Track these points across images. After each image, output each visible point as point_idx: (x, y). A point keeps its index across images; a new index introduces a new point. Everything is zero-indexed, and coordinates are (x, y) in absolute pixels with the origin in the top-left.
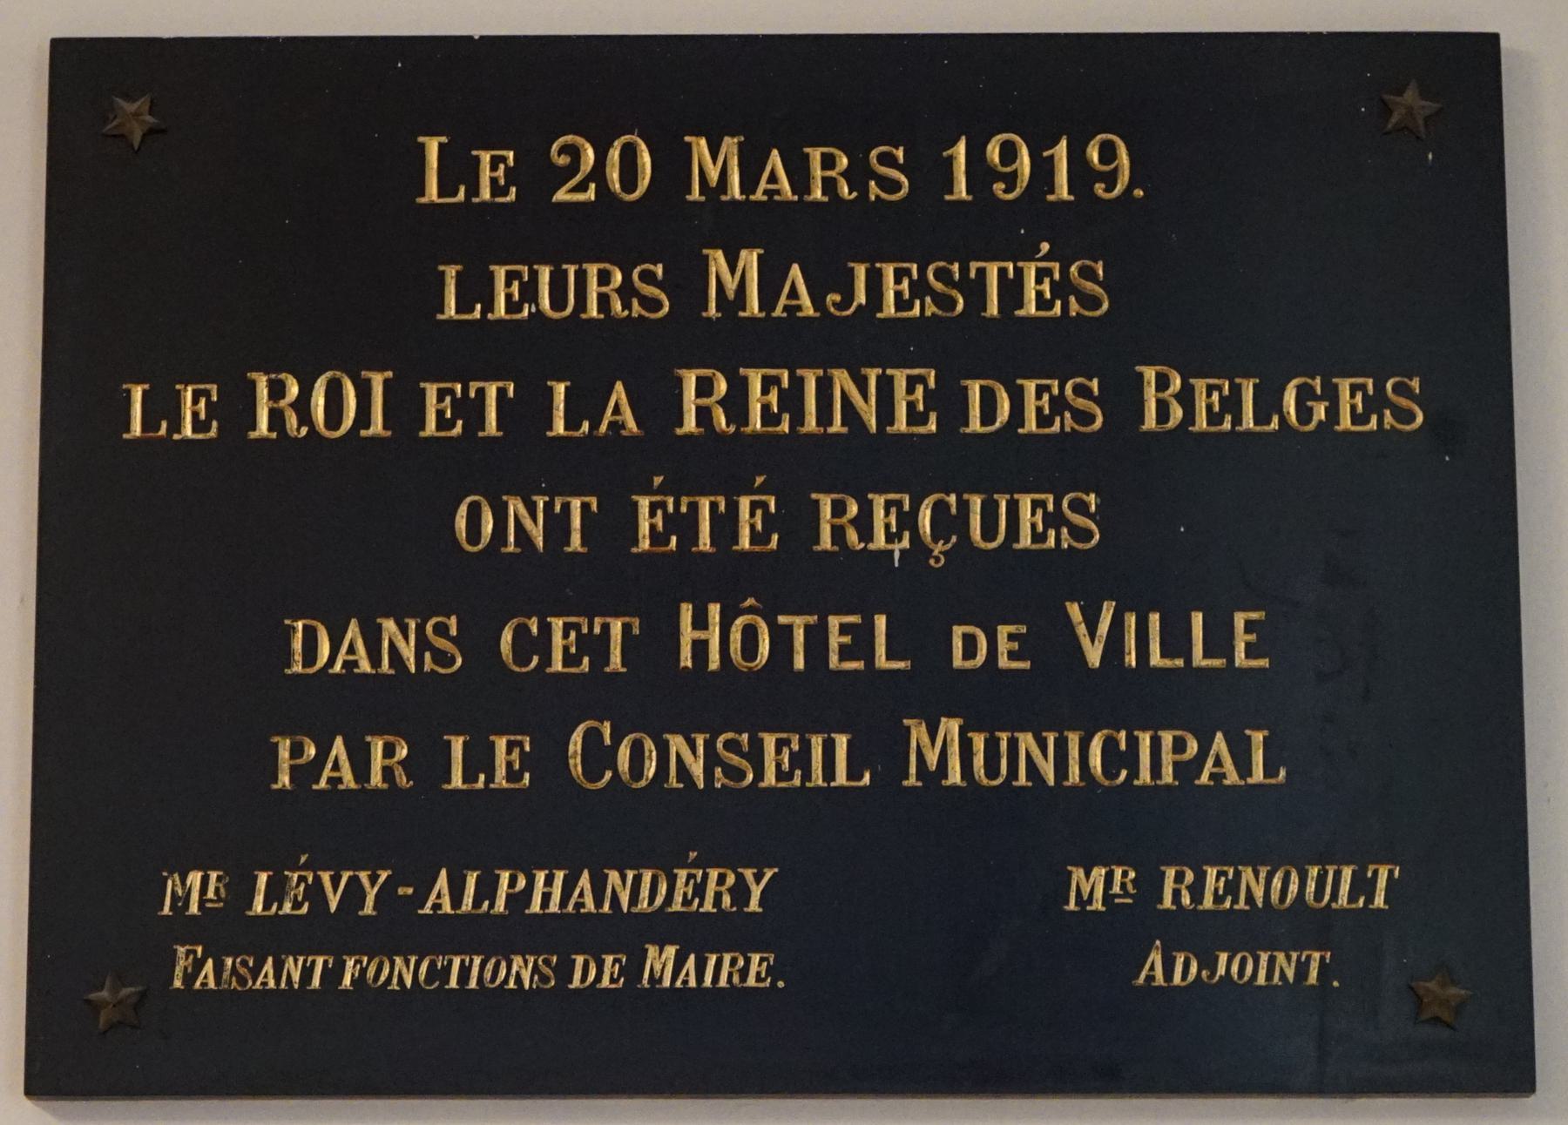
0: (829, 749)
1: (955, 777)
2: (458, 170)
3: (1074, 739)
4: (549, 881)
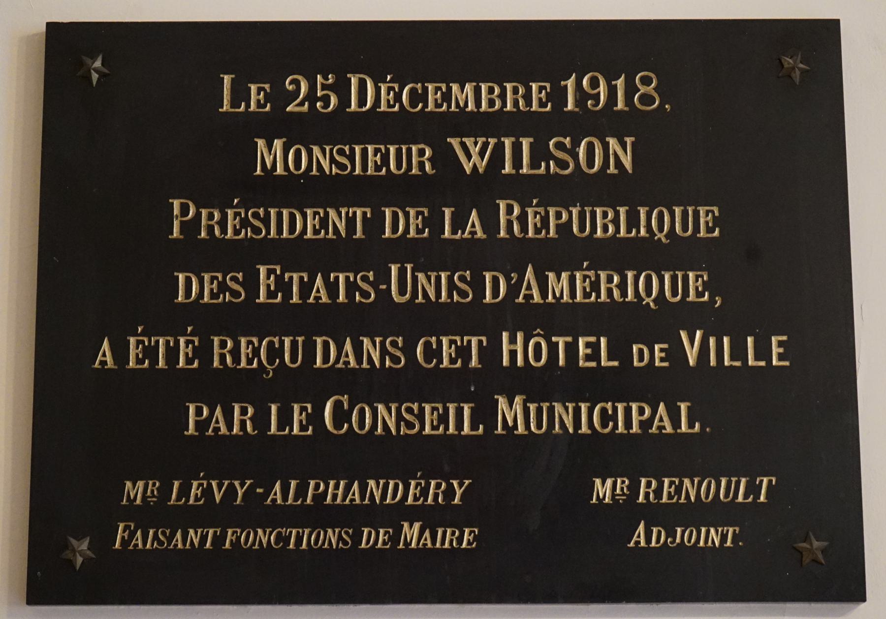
0: (459, 413)
1: (521, 429)
2: (240, 94)
3: (584, 407)
4: (337, 487)
